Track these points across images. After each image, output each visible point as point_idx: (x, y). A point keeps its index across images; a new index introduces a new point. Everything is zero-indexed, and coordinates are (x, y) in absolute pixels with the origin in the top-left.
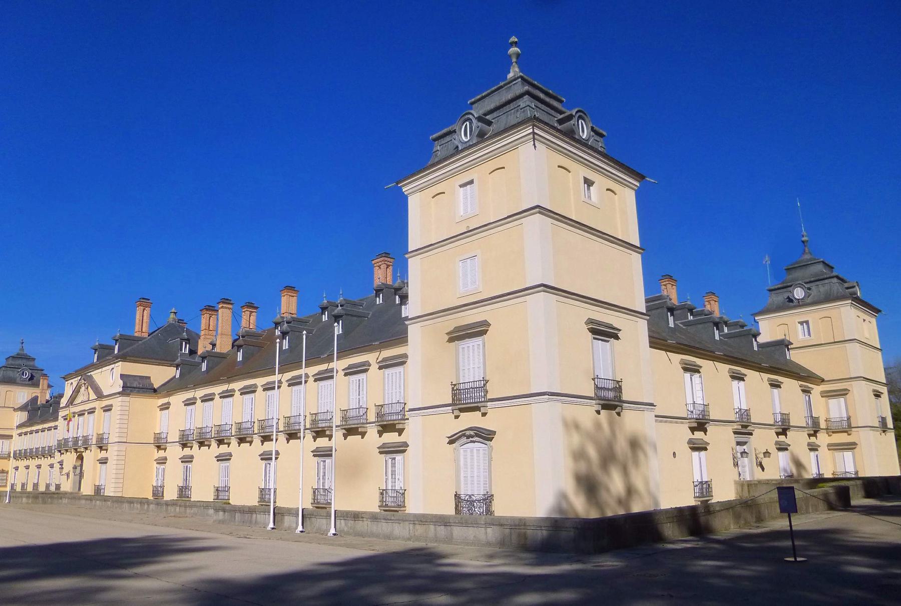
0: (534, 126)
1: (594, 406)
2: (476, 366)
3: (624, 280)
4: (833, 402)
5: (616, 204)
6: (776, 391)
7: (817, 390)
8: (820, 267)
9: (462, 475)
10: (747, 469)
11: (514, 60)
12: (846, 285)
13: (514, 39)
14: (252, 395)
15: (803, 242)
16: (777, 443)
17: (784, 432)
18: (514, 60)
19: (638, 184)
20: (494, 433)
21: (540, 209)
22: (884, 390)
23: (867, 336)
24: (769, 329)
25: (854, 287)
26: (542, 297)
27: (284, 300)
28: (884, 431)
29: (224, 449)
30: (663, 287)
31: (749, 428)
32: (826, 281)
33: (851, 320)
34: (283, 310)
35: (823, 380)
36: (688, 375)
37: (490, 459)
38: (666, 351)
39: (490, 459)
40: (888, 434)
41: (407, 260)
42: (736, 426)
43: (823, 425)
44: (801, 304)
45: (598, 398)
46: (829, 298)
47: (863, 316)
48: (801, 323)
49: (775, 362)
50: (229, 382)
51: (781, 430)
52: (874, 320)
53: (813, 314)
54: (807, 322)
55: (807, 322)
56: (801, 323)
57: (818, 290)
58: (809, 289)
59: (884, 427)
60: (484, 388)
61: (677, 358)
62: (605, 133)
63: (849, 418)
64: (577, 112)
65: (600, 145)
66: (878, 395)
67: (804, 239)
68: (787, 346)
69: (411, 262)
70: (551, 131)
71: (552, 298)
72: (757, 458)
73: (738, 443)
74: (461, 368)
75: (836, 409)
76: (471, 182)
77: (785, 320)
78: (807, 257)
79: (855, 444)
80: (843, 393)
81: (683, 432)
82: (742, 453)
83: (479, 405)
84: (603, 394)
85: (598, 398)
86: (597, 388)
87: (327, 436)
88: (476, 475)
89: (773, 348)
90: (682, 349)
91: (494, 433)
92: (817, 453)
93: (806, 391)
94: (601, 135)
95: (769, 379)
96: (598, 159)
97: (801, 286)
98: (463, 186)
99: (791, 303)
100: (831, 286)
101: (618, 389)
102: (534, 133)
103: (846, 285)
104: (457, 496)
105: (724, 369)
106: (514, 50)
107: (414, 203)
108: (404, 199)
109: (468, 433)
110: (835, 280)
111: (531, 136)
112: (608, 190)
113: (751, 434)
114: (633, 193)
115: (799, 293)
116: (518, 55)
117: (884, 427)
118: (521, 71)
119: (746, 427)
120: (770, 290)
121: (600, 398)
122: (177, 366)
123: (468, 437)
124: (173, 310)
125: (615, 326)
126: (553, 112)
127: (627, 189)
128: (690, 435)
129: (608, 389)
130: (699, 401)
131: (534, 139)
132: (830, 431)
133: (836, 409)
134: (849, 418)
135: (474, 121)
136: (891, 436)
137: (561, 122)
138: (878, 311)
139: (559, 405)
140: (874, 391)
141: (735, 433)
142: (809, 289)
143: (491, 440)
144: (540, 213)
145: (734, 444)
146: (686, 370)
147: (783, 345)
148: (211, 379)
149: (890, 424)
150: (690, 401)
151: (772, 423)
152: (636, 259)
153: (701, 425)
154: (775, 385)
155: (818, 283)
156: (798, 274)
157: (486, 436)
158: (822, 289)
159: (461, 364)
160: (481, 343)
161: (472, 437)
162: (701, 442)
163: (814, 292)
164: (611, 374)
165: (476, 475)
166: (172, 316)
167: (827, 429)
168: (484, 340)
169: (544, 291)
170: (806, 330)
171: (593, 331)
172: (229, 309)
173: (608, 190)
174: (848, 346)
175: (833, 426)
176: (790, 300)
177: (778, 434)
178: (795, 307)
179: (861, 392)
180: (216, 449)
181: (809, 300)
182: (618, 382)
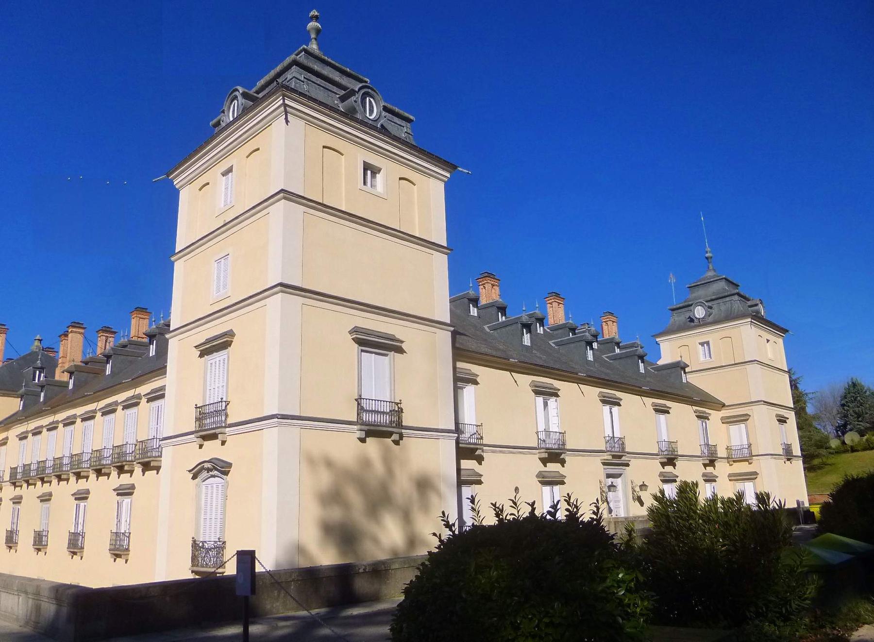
0: (284, 96)
1: (356, 432)
2: (221, 384)
3: (427, 285)
4: (734, 428)
5: (421, 198)
6: (662, 417)
7: (715, 416)
8: (722, 284)
9: (202, 517)
10: (621, 504)
11: (313, 36)
12: (749, 303)
13: (314, 13)
14: (73, 426)
15: (707, 258)
16: (704, 475)
17: (712, 463)
18: (313, 36)
19: (448, 175)
20: (230, 465)
21: (286, 194)
22: (791, 416)
23: (770, 355)
24: (669, 351)
25: (756, 305)
26: (278, 299)
27: (133, 322)
28: (789, 460)
29: (125, 479)
30: (549, 305)
31: (623, 458)
32: (728, 299)
33: (749, 339)
34: (133, 333)
35: (724, 405)
36: (540, 400)
37: (225, 497)
38: (511, 371)
39: (225, 497)
40: (794, 462)
41: (173, 263)
42: (607, 457)
43: (722, 452)
44: (702, 323)
45: (360, 422)
46: (730, 317)
47: (766, 335)
48: (702, 344)
49: (669, 387)
50: (55, 413)
51: (708, 462)
52: (780, 341)
53: (714, 335)
54: (708, 343)
55: (708, 343)
56: (702, 344)
57: (719, 308)
58: (710, 308)
59: (788, 455)
60: (224, 412)
61: (525, 380)
62: (412, 117)
63: (750, 446)
64: (360, 89)
65: (403, 131)
66: (782, 420)
67: (707, 255)
68: (683, 369)
69: (180, 267)
70: (311, 104)
71: (297, 300)
72: (634, 491)
73: (609, 476)
74: (208, 388)
75: (737, 436)
76: (230, 170)
77: (685, 341)
78: (711, 274)
79: (756, 473)
80: (744, 419)
81: (533, 464)
82: (609, 487)
83: (217, 431)
84: (366, 417)
85: (360, 422)
86: (361, 409)
87: (127, 472)
88: (213, 517)
89: (669, 371)
90: (536, 370)
91: (230, 465)
92: (714, 484)
93: (702, 417)
94: (408, 120)
95: (654, 405)
96: (387, 142)
97: (701, 304)
98: (225, 174)
99: (692, 323)
100: (737, 302)
101: (399, 412)
102: (285, 105)
103: (749, 303)
104: (195, 544)
105: (593, 392)
106: (313, 24)
107: (185, 197)
108: (175, 193)
109: (207, 465)
110: (736, 297)
111: (282, 108)
112: (400, 179)
113: (627, 465)
114: (442, 185)
115: (699, 312)
116: (318, 31)
117: (788, 455)
118: (320, 48)
119: (620, 457)
120: (673, 310)
121: (363, 424)
122: (22, 397)
123: (209, 470)
124: (38, 337)
125: (398, 336)
126: (335, 89)
127: (432, 180)
128: (540, 467)
129: (383, 413)
130: (554, 428)
131: (286, 113)
132: (731, 459)
133: (737, 436)
134: (750, 446)
135: (240, 98)
136: (798, 465)
137: (343, 99)
138: (785, 331)
139: (297, 430)
140: (777, 416)
141: (604, 464)
142: (710, 308)
143: (226, 473)
144: (285, 198)
145: (603, 477)
146: (537, 393)
147: (680, 367)
148: (53, 406)
149: (797, 451)
150: (541, 427)
151: (656, 452)
152: (441, 261)
153: (554, 456)
154: (662, 411)
155: (719, 301)
156: (701, 292)
157: (221, 468)
158: (723, 308)
159: (208, 383)
160: (226, 357)
161: (211, 470)
162: (557, 474)
163: (715, 311)
164: (388, 396)
165: (213, 517)
166: (37, 343)
167: (728, 458)
168: (228, 353)
169: (282, 292)
170: (707, 352)
171: (360, 342)
172: (79, 333)
173: (400, 179)
174: (748, 367)
175: (736, 455)
176: (692, 320)
177: (705, 465)
178: (699, 326)
179: (763, 417)
180: (115, 480)
181: (710, 319)
182: (397, 404)
